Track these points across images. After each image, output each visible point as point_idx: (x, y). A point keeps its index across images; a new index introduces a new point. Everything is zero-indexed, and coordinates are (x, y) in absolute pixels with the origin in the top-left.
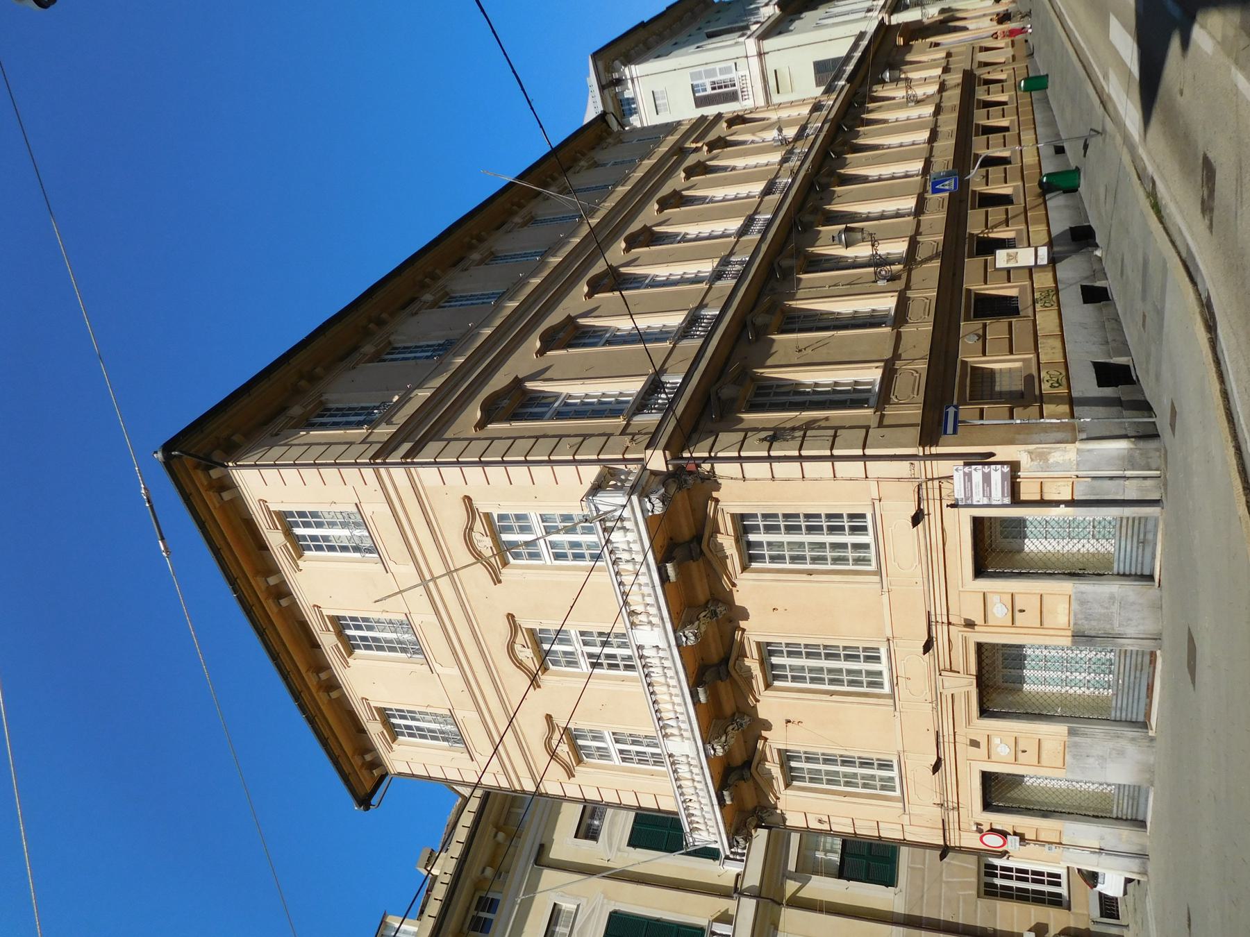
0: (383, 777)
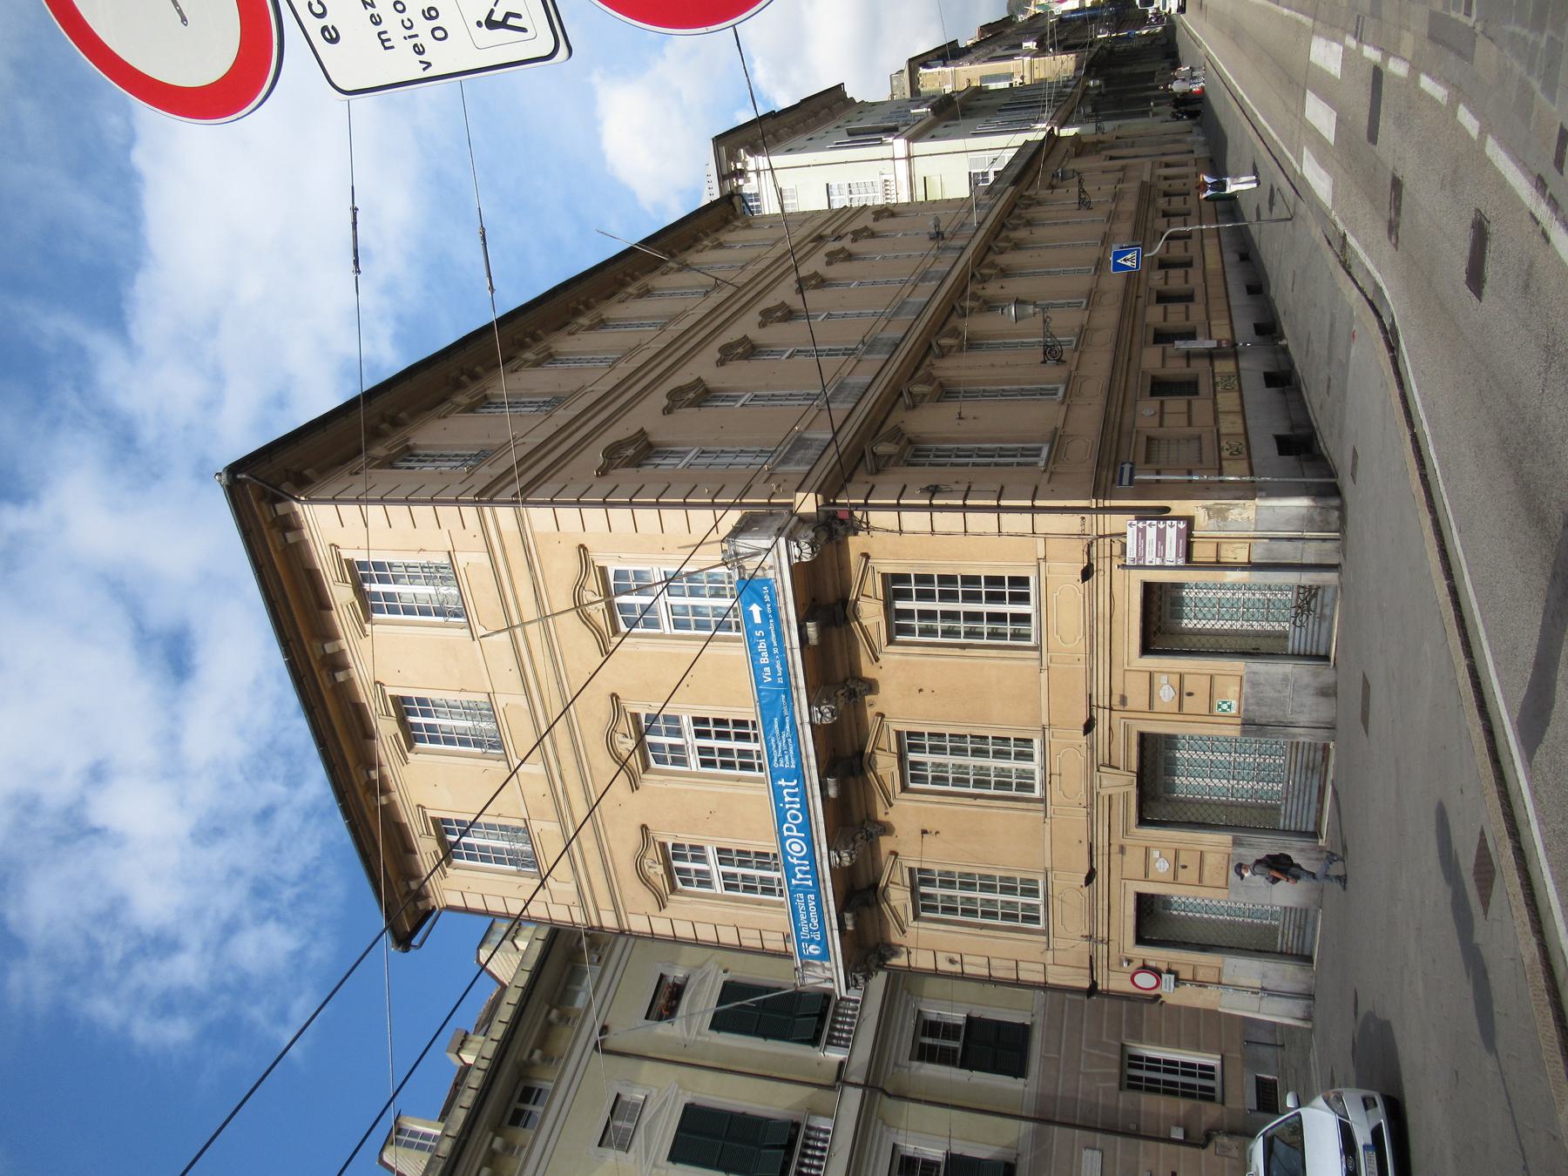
0: (428, 913)
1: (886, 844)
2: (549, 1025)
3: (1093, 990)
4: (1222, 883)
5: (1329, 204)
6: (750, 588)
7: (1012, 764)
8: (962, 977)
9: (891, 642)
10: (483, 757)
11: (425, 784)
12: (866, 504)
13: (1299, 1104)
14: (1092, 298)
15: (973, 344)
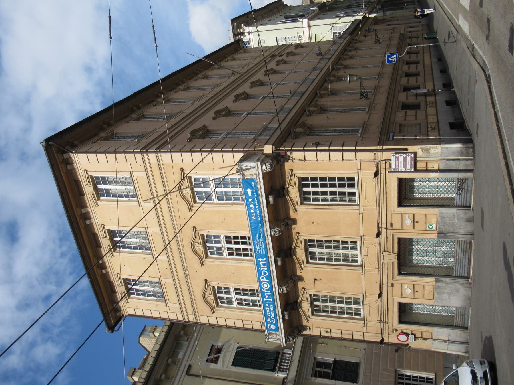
0: (120, 319)
1: (300, 285)
2: (168, 365)
3: (382, 341)
4: (432, 298)
5: (468, 34)
6: (247, 183)
7: (349, 252)
8: (331, 338)
9: (302, 204)
10: (143, 253)
11: (121, 265)
12: (291, 150)
13: (457, 367)
14: (380, 76)
15: (332, 93)
